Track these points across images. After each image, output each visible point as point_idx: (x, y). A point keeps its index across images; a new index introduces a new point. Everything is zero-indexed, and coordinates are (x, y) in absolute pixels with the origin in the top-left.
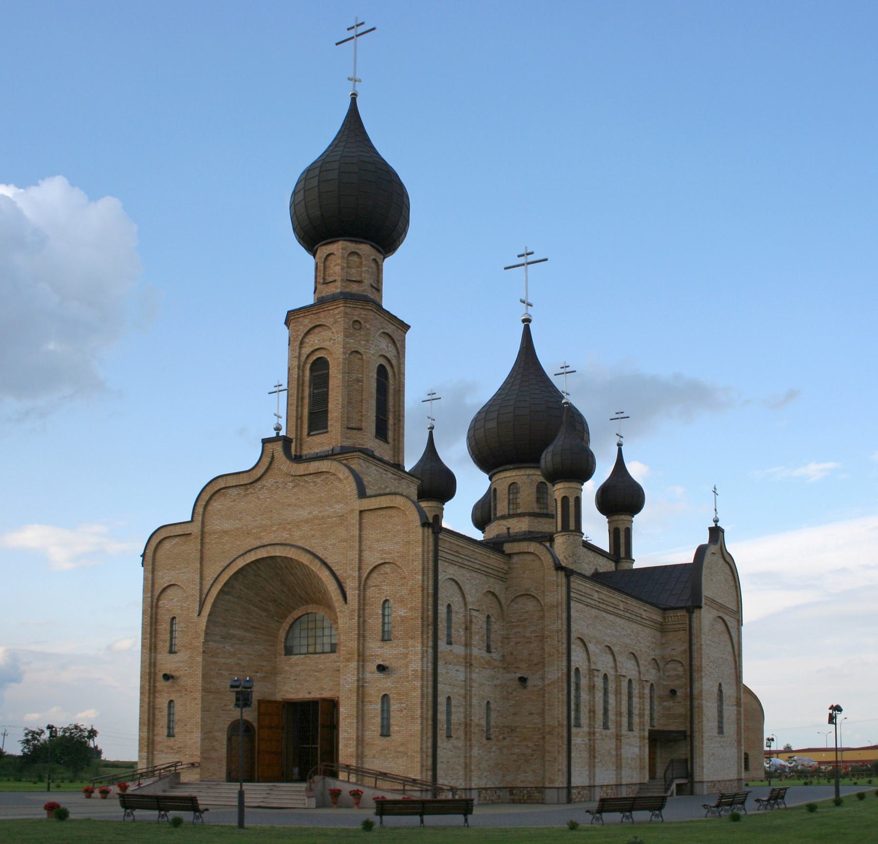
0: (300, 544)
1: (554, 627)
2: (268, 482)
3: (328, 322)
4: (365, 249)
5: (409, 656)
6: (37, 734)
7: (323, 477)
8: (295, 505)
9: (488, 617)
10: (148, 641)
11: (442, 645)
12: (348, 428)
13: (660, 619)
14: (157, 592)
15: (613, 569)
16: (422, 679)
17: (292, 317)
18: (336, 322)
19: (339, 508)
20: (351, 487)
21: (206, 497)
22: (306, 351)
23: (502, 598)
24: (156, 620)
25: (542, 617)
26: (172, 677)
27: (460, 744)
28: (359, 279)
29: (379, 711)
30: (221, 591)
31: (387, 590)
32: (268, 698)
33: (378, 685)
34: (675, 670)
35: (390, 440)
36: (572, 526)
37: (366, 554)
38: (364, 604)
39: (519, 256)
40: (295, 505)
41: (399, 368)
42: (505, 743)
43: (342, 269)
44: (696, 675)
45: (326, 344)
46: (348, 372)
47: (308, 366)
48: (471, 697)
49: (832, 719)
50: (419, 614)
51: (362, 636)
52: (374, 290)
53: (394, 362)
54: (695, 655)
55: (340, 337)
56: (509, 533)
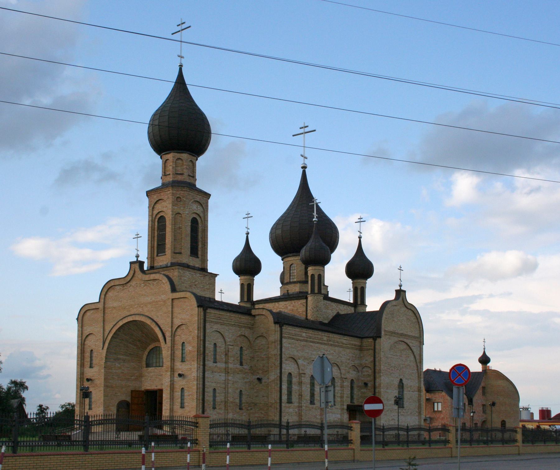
0: (147, 314)
1: (273, 353)
2: (133, 283)
3: (165, 198)
4: (185, 156)
5: (191, 368)
6: (44, 409)
7: (157, 281)
8: (145, 295)
9: (241, 348)
10: (79, 362)
11: (210, 363)
12: (174, 253)
14: (84, 338)
15: (353, 311)
16: (197, 380)
17: (149, 193)
18: (168, 198)
19: (163, 297)
21: (105, 290)
22: (155, 212)
24: (84, 351)
26: (91, 380)
27: (222, 412)
28: (182, 172)
29: (180, 396)
30: (112, 337)
32: (137, 389)
33: (180, 383)
34: (367, 371)
35: (200, 256)
36: (316, 291)
37: (175, 320)
38: (174, 344)
39: (301, 128)
40: (145, 295)
41: (205, 217)
42: (251, 411)
43: (173, 168)
44: (377, 375)
45: (164, 209)
46: (174, 223)
47: (157, 220)
48: (228, 388)
50: (196, 350)
51: (173, 360)
52: (190, 177)
53: (201, 215)
54: (377, 364)
55: (170, 206)
56: (288, 293)
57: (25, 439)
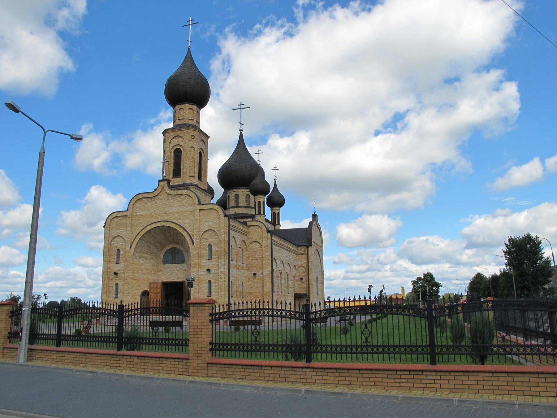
0: (174, 221)
1: (266, 254)
4: (195, 107)
13: (296, 250)
20: (196, 201)
22: (172, 145)
23: (246, 242)
25: (262, 250)
31: (210, 241)
36: (262, 213)
45: (181, 143)
47: (173, 151)
49: (369, 290)
57: (534, 343)
